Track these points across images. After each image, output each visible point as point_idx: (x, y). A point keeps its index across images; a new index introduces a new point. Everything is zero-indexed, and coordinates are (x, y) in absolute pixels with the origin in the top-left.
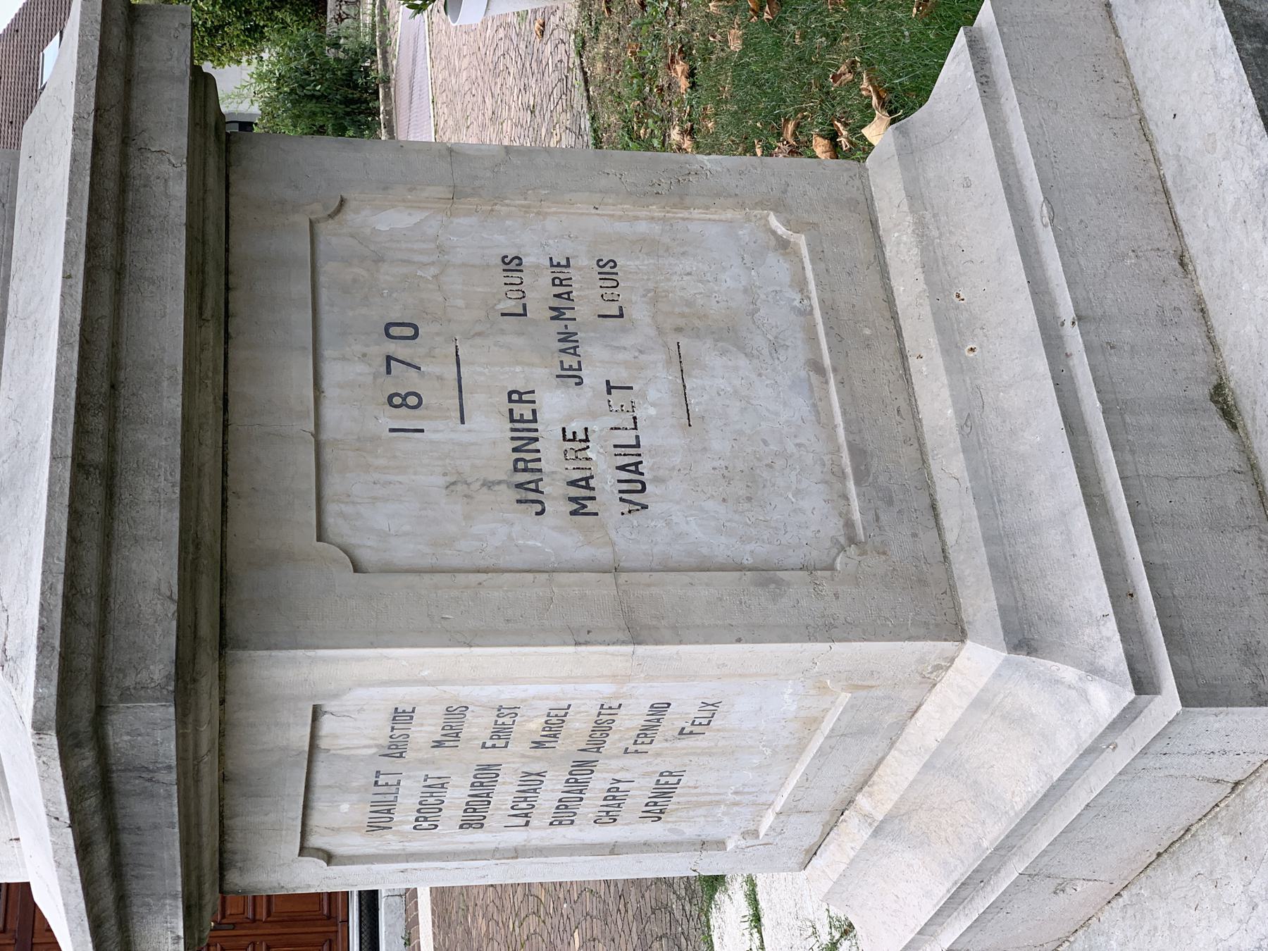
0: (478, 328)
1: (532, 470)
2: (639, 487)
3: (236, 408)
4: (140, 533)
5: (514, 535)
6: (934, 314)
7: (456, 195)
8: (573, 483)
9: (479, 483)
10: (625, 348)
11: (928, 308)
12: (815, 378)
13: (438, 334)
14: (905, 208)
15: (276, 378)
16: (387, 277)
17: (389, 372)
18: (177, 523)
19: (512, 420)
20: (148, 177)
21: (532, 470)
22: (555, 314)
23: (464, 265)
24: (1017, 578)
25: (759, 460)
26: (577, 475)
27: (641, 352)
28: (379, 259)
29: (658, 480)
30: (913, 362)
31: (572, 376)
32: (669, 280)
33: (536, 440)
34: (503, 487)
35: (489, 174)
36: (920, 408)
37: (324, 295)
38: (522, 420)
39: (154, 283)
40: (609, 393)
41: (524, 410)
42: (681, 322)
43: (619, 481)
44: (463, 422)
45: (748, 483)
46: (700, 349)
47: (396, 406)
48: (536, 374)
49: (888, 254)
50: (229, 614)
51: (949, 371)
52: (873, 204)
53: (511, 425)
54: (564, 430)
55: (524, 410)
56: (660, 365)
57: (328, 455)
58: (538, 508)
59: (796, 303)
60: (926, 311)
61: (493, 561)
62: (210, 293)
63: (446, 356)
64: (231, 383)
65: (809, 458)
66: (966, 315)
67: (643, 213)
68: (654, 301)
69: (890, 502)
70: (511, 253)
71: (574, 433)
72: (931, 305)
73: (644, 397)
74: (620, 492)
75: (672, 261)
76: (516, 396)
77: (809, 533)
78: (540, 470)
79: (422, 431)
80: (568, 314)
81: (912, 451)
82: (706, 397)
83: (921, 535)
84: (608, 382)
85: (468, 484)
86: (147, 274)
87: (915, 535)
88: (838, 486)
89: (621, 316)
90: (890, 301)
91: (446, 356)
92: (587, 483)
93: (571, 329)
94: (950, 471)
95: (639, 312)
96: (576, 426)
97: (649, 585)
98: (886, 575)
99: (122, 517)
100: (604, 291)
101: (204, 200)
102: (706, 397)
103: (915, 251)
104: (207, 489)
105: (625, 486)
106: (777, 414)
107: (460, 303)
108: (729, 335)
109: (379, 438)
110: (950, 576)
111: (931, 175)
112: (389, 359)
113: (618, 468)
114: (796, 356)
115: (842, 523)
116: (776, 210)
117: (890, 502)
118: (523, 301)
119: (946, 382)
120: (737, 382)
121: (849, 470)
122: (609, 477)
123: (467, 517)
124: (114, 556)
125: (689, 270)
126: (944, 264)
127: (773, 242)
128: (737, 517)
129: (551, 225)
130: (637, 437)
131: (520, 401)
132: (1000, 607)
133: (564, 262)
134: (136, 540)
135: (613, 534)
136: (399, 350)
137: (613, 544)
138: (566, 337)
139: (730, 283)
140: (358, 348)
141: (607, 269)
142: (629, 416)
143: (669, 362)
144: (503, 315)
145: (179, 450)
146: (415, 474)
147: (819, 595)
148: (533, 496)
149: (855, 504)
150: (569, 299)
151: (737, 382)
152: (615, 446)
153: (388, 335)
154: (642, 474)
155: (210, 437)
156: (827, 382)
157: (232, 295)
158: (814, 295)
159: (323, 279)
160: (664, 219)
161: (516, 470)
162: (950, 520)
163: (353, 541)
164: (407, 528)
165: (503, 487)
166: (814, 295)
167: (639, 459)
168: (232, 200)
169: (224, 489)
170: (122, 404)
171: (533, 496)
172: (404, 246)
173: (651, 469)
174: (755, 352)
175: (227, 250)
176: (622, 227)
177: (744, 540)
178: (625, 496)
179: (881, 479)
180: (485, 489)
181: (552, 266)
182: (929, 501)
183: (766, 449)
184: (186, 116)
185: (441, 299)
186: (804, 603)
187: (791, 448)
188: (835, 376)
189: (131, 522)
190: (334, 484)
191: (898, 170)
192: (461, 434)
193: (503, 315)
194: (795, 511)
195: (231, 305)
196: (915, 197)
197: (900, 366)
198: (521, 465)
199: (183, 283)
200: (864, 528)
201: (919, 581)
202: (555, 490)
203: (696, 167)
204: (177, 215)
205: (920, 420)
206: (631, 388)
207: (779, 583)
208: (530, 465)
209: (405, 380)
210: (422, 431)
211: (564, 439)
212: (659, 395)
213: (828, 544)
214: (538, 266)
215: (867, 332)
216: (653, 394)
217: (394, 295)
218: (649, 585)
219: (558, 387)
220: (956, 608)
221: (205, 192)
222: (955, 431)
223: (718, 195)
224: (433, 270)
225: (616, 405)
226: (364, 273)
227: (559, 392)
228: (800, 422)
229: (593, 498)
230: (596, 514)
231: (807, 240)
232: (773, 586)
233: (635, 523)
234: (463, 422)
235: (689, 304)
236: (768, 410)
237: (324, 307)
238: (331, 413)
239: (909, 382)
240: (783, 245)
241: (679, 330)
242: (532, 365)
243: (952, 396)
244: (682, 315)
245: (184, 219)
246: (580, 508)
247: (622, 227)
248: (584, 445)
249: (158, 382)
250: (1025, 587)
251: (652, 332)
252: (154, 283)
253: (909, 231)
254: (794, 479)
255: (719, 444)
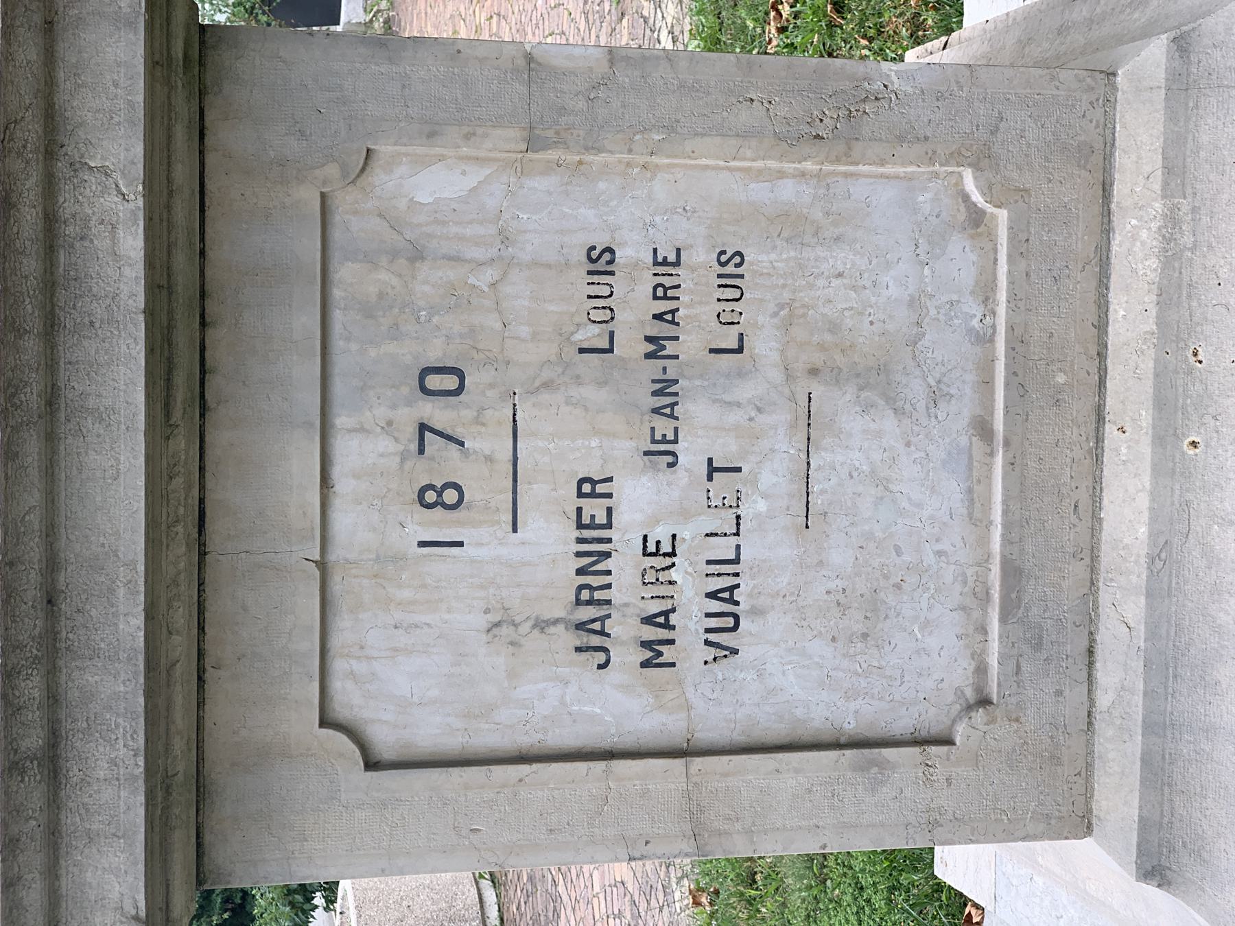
0: (546, 374)
1: (600, 603)
2: (730, 622)
3: (217, 527)
4: (94, 827)
5: (568, 699)
6: (1157, 375)
7: (533, 143)
8: (648, 620)
9: (530, 623)
10: (739, 405)
11: (1151, 364)
12: (978, 446)
13: (492, 386)
14: (1157, 187)
15: (270, 476)
16: (426, 288)
17: (421, 451)
18: (142, 811)
19: (580, 526)
20: (87, 219)
21: (600, 603)
22: (652, 348)
23: (535, 264)
24: (1170, 785)
25: (886, 577)
26: (655, 607)
27: (759, 410)
28: (417, 255)
29: (756, 612)
30: (1110, 430)
31: (663, 452)
32: (811, 286)
33: (608, 555)
34: (560, 628)
35: (581, 104)
36: (1105, 502)
37: (338, 317)
38: (592, 526)
39: (102, 420)
40: (710, 478)
41: (593, 509)
42: (818, 359)
43: (708, 615)
44: (515, 530)
45: (864, 615)
46: (837, 402)
47: (429, 506)
48: (614, 449)
49: (1115, 248)
50: (208, 838)
51: (1156, 470)
52: (1112, 154)
53: (577, 534)
54: (645, 537)
55: (593, 509)
56: (781, 431)
57: (337, 585)
58: (601, 657)
59: (975, 323)
60: (1148, 366)
61: (540, 736)
62: (180, 379)
63: (499, 423)
64: (209, 485)
65: (949, 574)
66: (1199, 387)
67: (789, 167)
68: (787, 325)
69: (1038, 646)
70: (601, 241)
71: (658, 543)
72: (1156, 361)
73: (754, 482)
74: (708, 631)
75: (820, 252)
76: (589, 487)
77: (929, 684)
78: (608, 602)
79: (460, 544)
80: (670, 348)
81: (1079, 569)
82: (834, 481)
83: (1067, 693)
84: (710, 460)
85: (516, 625)
86: (91, 403)
87: (1059, 693)
88: (976, 614)
89: (740, 350)
90: (1101, 326)
91: (499, 423)
92: (667, 619)
93: (671, 375)
94: (1123, 611)
95: (764, 345)
96: (661, 533)
97: (726, 775)
98: (1014, 750)
99: (71, 804)
100: (724, 305)
101: (169, 207)
102: (834, 481)
103: (1153, 263)
104: (179, 700)
105: (713, 623)
106: (919, 505)
107: (524, 331)
108: (877, 380)
109: (405, 558)
110: (1090, 753)
111: (1204, 139)
112: (423, 428)
113: (708, 595)
114: (957, 417)
115: (971, 668)
116: (976, 167)
117: (1038, 646)
118: (610, 326)
119: (1148, 485)
120: (876, 456)
121: (996, 596)
122: (695, 609)
123: (512, 675)
124: (62, 862)
125: (840, 268)
126: (1189, 296)
127: (962, 216)
128: (846, 663)
129: (660, 188)
130: (738, 547)
131: (593, 495)
132: (1141, 818)
133: (672, 258)
134: (91, 838)
135: (690, 693)
136: (438, 413)
137: (689, 708)
138: (664, 387)
139: (894, 291)
140: (382, 412)
141: (730, 269)
142: (730, 515)
143: (793, 426)
144: (582, 351)
145: (142, 700)
146: (449, 611)
147: (928, 781)
148: (596, 641)
149: (994, 646)
150: (673, 322)
151: (876, 456)
152: (709, 562)
153: (424, 390)
154: (737, 603)
155: (182, 617)
156: (992, 454)
157: (211, 334)
158: (1002, 310)
159: (337, 293)
160: (819, 175)
161: (578, 602)
162: (1108, 676)
163: (366, 714)
164: (434, 693)
165: (560, 628)
166: (1002, 310)
167: (735, 581)
168: (210, 159)
169: (201, 654)
170: (63, 625)
171: (596, 641)
172: (454, 229)
173: (750, 595)
174: (908, 406)
175: (202, 469)
176: (759, 192)
177: (849, 695)
178: (713, 637)
179: (1035, 610)
180: (536, 632)
181: (656, 263)
182: (1086, 643)
183: (898, 561)
184: (140, 98)
185: (499, 326)
186: (908, 793)
187: (930, 559)
188: (1005, 452)
189: (83, 811)
190: (344, 632)
191: (1160, 116)
192: (510, 548)
193: (582, 351)
194: (918, 652)
195: (208, 354)
196: (1176, 173)
197: (1093, 434)
198: (585, 595)
199: (142, 417)
200: (999, 685)
201: (1052, 757)
202: (625, 630)
203: (878, 85)
204: (132, 295)
205: (1100, 520)
206: (739, 470)
207: (882, 765)
208: (598, 595)
209: (445, 464)
210: (460, 544)
211: (645, 554)
212: (775, 480)
213: (951, 698)
214: (636, 265)
215: (1061, 379)
216: (767, 479)
217: (435, 319)
218: (726, 775)
219: (644, 471)
220: (1088, 795)
221: (171, 193)
222: (1143, 560)
223: (901, 139)
224: (490, 274)
225: (716, 496)
226: (395, 281)
227: (644, 479)
228: (947, 518)
229: (671, 642)
230: (673, 665)
231: (1009, 219)
232: (875, 770)
233: (720, 677)
234: (515, 530)
235: (834, 327)
236: (909, 499)
237: (338, 343)
238: (344, 520)
239: (1098, 460)
240: (976, 218)
241: (814, 372)
242: (614, 435)
243: (1151, 509)
244: (822, 347)
245: (141, 301)
246: (654, 656)
247: (759, 192)
248: (668, 561)
249: (111, 591)
250: (1178, 801)
251: (776, 376)
252: (102, 420)
253: (1154, 226)
254: (924, 605)
255: (840, 556)
